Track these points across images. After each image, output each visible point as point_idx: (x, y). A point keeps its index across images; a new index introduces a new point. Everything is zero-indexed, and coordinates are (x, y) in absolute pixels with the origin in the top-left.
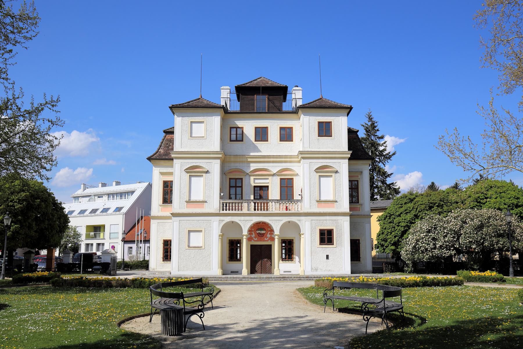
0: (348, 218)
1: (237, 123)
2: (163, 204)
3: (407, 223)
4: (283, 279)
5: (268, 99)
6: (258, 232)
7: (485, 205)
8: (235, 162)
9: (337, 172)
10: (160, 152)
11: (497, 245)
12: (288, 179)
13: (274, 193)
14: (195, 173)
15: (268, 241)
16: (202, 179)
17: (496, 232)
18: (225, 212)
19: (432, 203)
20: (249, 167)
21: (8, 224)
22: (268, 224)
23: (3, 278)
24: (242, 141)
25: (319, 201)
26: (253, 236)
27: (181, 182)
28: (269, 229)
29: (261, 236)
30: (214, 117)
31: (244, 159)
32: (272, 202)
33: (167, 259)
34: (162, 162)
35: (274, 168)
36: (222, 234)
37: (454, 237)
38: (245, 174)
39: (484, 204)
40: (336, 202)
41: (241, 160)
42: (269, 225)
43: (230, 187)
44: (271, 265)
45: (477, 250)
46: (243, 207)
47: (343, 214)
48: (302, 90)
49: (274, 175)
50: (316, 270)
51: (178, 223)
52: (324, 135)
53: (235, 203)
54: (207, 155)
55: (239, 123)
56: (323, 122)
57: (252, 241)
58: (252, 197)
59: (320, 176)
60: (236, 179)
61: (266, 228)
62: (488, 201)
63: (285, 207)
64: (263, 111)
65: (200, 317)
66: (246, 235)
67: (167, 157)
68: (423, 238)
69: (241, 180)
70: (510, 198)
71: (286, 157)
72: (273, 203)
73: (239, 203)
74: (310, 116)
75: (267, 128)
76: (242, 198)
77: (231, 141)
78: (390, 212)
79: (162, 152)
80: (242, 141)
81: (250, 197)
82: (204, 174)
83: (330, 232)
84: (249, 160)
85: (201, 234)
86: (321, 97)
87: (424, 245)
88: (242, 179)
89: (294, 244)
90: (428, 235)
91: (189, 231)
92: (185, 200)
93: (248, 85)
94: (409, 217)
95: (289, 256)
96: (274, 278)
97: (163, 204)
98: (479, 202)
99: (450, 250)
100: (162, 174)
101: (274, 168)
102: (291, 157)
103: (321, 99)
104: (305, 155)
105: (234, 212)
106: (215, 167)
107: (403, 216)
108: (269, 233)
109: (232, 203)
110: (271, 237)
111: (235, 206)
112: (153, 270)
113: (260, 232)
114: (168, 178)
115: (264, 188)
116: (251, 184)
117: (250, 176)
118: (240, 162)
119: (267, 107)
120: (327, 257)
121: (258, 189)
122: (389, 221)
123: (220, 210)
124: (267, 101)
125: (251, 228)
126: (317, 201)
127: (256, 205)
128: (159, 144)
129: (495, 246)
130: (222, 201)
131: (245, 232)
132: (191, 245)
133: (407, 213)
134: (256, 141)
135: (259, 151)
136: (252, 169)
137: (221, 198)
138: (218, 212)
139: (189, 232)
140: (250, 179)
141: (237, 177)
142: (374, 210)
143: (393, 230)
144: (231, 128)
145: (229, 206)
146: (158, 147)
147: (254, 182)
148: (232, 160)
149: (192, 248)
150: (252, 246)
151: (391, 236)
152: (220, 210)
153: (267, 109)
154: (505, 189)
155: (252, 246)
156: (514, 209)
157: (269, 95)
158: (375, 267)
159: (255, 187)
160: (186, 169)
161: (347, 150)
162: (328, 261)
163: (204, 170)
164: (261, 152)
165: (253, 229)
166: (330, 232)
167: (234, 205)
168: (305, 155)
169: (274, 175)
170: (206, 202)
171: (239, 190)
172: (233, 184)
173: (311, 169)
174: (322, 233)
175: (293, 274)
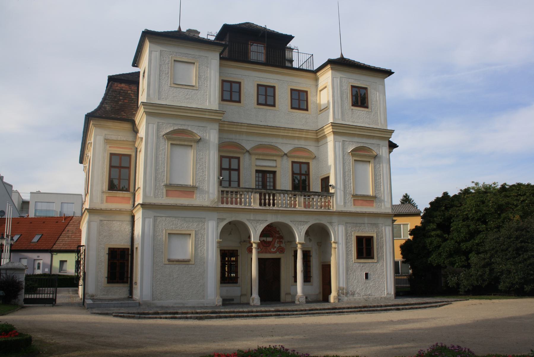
10: (105, 108)
18: (225, 205)
24: (239, 102)
41: (239, 130)
60: (230, 158)
69: (237, 160)
79: (108, 108)
88: (238, 158)
108: (276, 242)
110: (280, 246)
131: (255, 238)
148: (226, 129)
149: (175, 263)
160: (167, 134)
162: (367, 281)
171: (234, 174)
172: (226, 165)
174: (360, 240)
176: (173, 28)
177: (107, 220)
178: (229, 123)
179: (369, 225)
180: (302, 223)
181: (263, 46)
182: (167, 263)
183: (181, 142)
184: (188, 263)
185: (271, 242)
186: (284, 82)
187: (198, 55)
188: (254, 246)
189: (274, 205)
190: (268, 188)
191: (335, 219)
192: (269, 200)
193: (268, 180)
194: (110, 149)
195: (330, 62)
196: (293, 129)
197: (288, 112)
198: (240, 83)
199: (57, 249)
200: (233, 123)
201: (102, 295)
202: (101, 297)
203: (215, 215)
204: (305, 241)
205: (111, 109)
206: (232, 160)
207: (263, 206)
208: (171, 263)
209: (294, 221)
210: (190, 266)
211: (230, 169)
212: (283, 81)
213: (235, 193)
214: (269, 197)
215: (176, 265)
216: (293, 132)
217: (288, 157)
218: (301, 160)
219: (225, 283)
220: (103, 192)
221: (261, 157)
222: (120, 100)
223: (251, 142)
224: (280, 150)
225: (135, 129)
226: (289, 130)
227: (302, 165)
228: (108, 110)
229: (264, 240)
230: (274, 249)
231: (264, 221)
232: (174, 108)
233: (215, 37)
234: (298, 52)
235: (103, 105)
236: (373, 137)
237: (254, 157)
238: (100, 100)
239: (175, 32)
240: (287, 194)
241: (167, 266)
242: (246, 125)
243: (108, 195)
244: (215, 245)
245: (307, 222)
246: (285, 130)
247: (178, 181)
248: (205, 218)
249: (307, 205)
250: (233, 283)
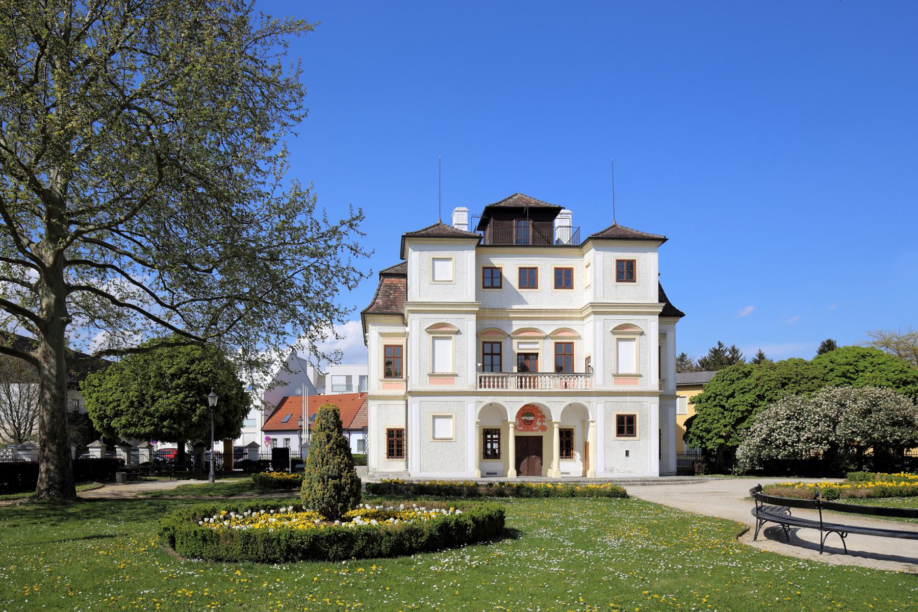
0: (657, 399)
1: (492, 261)
2: (385, 378)
3: (747, 406)
5: (533, 226)
6: (524, 418)
7: (857, 381)
8: (491, 318)
9: (642, 334)
10: (378, 303)
11: (891, 437)
12: (565, 343)
13: (546, 363)
14: (440, 334)
15: (537, 431)
16: (450, 342)
17: (892, 418)
18: (483, 389)
19: (785, 378)
20: (511, 325)
21: (213, 404)
23: (213, 481)
24: (501, 287)
25: (616, 376)
27: (421, 346)
28: (539, 414)
29: (528, 424)
30: (466, 252)
31: (504, 314)
32: (545, 377)
33: (393, 455)
34: (382, 318)
35: (547, 328)
37: (829, 426)
38: (506, 336)
39: (855, 380)
40: (640, 376)
41: (500, 316)
44: (542, 464)
45: (862, 445)
46: (508, 384)
47: (651, 394)
48: (468, 212)
49: (546, 338)
50: (612, 471)
51: (417, 405)
52: (625, 279)
53: (498, 377)
54: (457, 308)
55: (496, 262)
56: (623, 261)
58: (515, 369)
59: (618, 340)
60: (492, 343)
61: (534, 412)
62: (861, 376)
63: (564, 384)
64: (509, 244)
65: (842, 537)
67: (389, 311)
68: (781, 427)
69: (499, 345)
70: (894, 372)
71: (564, 311)
72: (547, 377)
73: (498, 377)
74: (605, 251)
75: (536, 269)
76: (501, 371)
78: (715, 391)
80: (501, 287)
81: (512, 369)
82: (453, 336)
83: (631, 419)
84: (511, 316)
85: (451, 421)
86: (614, 224)
87: (781, 436)
88: (500, 343)
90: (788, 423)
91: (433, 416)
92: (428, 373)
93: (502, 204)
94: (750, 397)
95: (567, 451)
97: (385, 378)
98: (850, 378)
99: (821, 444)
100: (382, 335)
101: (547, 328)
102: (572, 312)
103: (614, 226)
104: (598, 309)
105: (487, 389)
106: (469, 325)
107: (739, 397)
109: (494, 377)
110: (542, 425)
111: (498, 382)
113: (526, 418)
115: (531, 357)
116: (513, 351)
117: (512, 338)
118: (497, 318)
119: (531, 237)
120: (627, 453)
121: (523, 357)
122: (714, 403)
123: (477, 387)
124: (531, 228)
126: (614, 376)
128: (375, 291)
129: (888, 438)
130: (479, 375)
131: (512, 417)
132: (437, 436)
133: (745, 392)
134: (520, 287)
135: (525, 303)
136: (515, 329)
137: (477, 369)
138: (474, 390)
139: (434, 417)
140: (512, 343)
141: (493, 340)
142: (681, 387)
143: (720, 416)
145: (485, 382)
146: (373, 296)
147: (518, 347)
148: (487, 316)
149: (439, 440)
151: (718, 425)
152: (477, 387)
153: (531, 241)
154: (883, 360)
156: (900, 387)
157: (534, 220)
159: (519, 354)
161: (657, 301)
162: (628, 458)
163: (454, 330)
164: (527, 303)
166: (631, 419)
167: (500, 380)
168: (598, 309)
169: (546, 338)
170: (457, 375)
171: (496, 358)
172: (488, 351)
173: (605, 329)
174: (620, 419)
175: (573, 476)
188: (511, 425)
189: (530, 387)
192: (526, 382)
195: (590, 238)
199: (354, 428)
203: (474, 399)
206: (494, 345)
211: (492, 354)
214: (526, 379)
222: (390, 294)
225: (405, 322)
244: (474, 425)
250: (496, 458)
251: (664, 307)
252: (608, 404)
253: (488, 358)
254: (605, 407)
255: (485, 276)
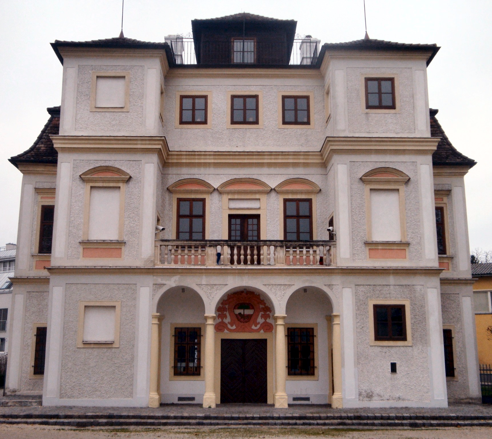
4: (302, 421)
15: (258, 331)
22: (259, 295)
26: (227, 320)
36: (158, 314)
41: (202, 161)
42: (261, 298)
43: (179, 216)
50: (370, 396)
57: (226, 331)
66: (214, 318)
72: (272, 248)
77: (182, 122)
79: (42, 148)
88: (203, 200)
89: (315, 338)
96: (279, 418)
105: (242, 266)
108: (260, 315)
112: (13, 394)
113: (241, 311)
114: (47, 202)
120: (394, 368)
121: (238, 221)
125: (222, 304)
127: (235, 251)
131: (210, 311)
144: (182, 97)
149: (92, 346)
150: (223, 340)
155: (223, 340)
158: (485, 385)
161: (429, 135)
162: (395, 376)
165: (227, 306)
171: (304, 222)
172: (292, 211)
176: (113, 34)
177: (36, 292)
178: (188, 153)
179: (397, 287)
180: (282, 287)
181: (253, 41)
182: (82, 346)
183: (104, 183)
184: (110, 346)
185: (252, 315)
186: (272, 88)
187: (130, 66)
189: (239, 262)
190: (250, 238)
191: (337, 280)
193: (250, 227)
194: (43, 200)
196: (284, 153)
197: (278, 129)
198: (205, 97)
200: (193, 153)
201: (27, 390)
202: (25, 392)
203: (150, 280)
204: (286, 314)
205: (47, 150)
207: (249, 264)
208: (86, 346)
209: (269, 285)
210: (113, 350)
211: (298, 217)
212: (271, 86)
213: (188, 248)
214: (252, 251)
215: (94, 350)
216: (283, 157)
217: (277, 193)
218: (193, 196)
219: (295, 374)
220: (33, 256)
221: (236, 197)
223: (222, 176)
224: (267, 186)
226: (278, 155)
227: (301, 204)
228: (41, 151)
229: (240, 314)
230: (256, 326)
231: (222, 286)
232: (394, 141)
233: (295, 39)
234: (176, 42)
235: (37, 146)
236: (403, 152)
237: (225, 197)
238: (35, 139)
239: (363, 40)
240: (220, 246)
241: (82, 350)
242: (212, 153)
243: (38, 259)
245: (290, 285)
246: (271, 155)
247: (96, 235)
248: (136, 284)
249: (291, 260)
251: (439, 142)
252: (361, 288)
253: (185, 222)
254: (356, 294)
255: (306, 112)
